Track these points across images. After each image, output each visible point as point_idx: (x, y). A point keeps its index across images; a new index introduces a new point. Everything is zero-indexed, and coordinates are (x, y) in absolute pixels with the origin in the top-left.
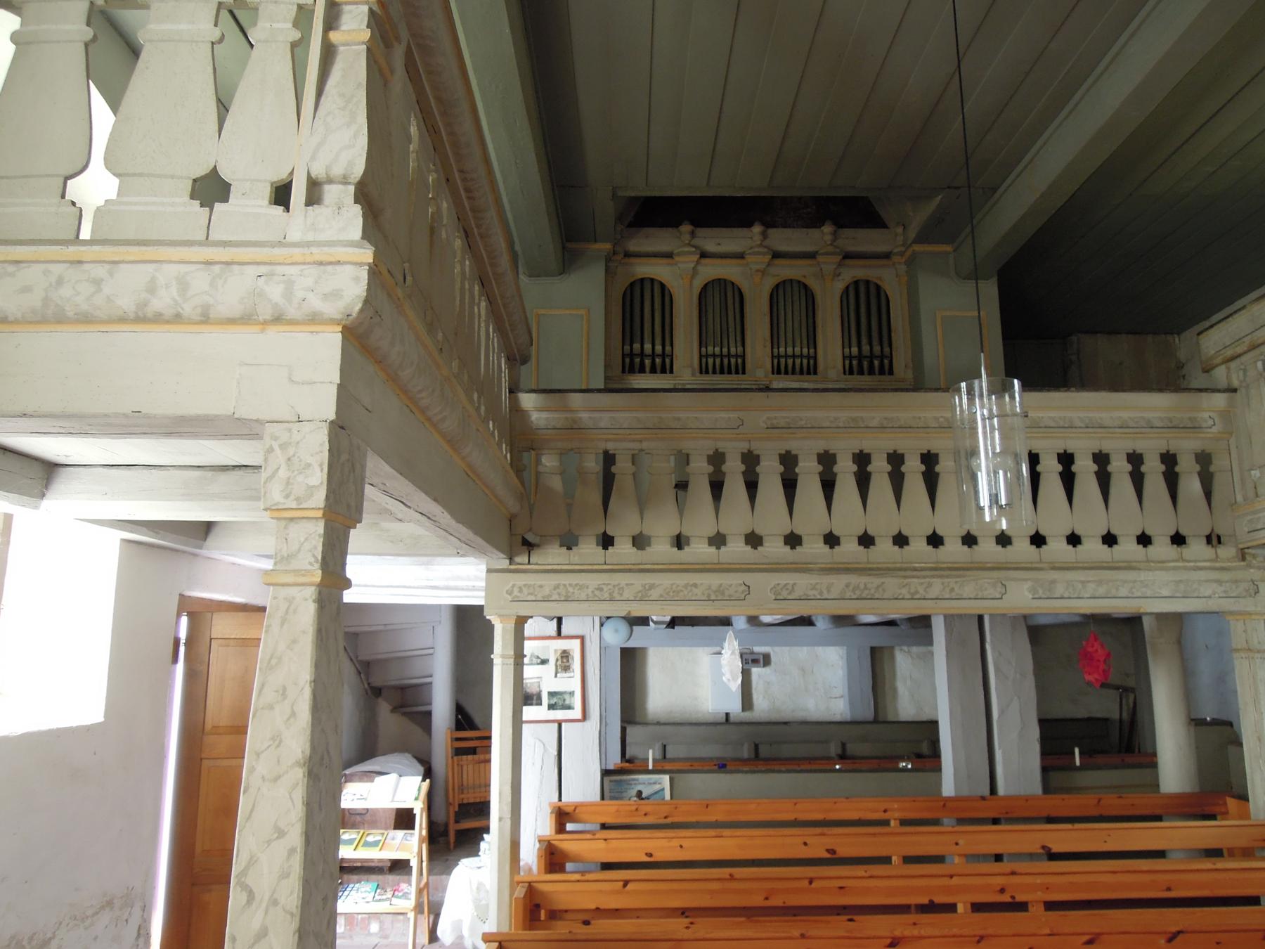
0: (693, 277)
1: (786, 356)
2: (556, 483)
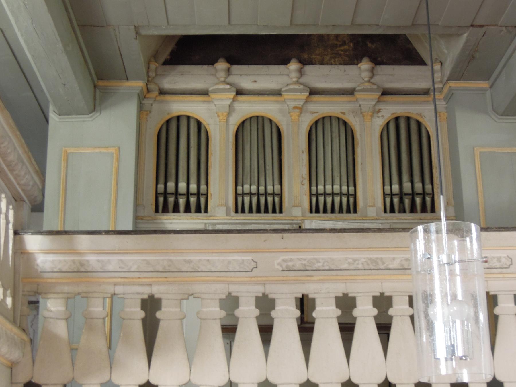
0: (229, 114)
1: (325, 194)
2: (61, 329)
